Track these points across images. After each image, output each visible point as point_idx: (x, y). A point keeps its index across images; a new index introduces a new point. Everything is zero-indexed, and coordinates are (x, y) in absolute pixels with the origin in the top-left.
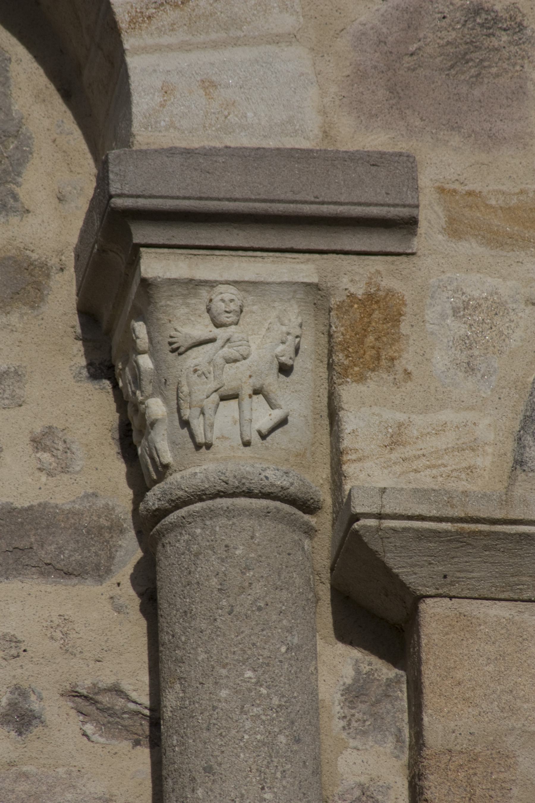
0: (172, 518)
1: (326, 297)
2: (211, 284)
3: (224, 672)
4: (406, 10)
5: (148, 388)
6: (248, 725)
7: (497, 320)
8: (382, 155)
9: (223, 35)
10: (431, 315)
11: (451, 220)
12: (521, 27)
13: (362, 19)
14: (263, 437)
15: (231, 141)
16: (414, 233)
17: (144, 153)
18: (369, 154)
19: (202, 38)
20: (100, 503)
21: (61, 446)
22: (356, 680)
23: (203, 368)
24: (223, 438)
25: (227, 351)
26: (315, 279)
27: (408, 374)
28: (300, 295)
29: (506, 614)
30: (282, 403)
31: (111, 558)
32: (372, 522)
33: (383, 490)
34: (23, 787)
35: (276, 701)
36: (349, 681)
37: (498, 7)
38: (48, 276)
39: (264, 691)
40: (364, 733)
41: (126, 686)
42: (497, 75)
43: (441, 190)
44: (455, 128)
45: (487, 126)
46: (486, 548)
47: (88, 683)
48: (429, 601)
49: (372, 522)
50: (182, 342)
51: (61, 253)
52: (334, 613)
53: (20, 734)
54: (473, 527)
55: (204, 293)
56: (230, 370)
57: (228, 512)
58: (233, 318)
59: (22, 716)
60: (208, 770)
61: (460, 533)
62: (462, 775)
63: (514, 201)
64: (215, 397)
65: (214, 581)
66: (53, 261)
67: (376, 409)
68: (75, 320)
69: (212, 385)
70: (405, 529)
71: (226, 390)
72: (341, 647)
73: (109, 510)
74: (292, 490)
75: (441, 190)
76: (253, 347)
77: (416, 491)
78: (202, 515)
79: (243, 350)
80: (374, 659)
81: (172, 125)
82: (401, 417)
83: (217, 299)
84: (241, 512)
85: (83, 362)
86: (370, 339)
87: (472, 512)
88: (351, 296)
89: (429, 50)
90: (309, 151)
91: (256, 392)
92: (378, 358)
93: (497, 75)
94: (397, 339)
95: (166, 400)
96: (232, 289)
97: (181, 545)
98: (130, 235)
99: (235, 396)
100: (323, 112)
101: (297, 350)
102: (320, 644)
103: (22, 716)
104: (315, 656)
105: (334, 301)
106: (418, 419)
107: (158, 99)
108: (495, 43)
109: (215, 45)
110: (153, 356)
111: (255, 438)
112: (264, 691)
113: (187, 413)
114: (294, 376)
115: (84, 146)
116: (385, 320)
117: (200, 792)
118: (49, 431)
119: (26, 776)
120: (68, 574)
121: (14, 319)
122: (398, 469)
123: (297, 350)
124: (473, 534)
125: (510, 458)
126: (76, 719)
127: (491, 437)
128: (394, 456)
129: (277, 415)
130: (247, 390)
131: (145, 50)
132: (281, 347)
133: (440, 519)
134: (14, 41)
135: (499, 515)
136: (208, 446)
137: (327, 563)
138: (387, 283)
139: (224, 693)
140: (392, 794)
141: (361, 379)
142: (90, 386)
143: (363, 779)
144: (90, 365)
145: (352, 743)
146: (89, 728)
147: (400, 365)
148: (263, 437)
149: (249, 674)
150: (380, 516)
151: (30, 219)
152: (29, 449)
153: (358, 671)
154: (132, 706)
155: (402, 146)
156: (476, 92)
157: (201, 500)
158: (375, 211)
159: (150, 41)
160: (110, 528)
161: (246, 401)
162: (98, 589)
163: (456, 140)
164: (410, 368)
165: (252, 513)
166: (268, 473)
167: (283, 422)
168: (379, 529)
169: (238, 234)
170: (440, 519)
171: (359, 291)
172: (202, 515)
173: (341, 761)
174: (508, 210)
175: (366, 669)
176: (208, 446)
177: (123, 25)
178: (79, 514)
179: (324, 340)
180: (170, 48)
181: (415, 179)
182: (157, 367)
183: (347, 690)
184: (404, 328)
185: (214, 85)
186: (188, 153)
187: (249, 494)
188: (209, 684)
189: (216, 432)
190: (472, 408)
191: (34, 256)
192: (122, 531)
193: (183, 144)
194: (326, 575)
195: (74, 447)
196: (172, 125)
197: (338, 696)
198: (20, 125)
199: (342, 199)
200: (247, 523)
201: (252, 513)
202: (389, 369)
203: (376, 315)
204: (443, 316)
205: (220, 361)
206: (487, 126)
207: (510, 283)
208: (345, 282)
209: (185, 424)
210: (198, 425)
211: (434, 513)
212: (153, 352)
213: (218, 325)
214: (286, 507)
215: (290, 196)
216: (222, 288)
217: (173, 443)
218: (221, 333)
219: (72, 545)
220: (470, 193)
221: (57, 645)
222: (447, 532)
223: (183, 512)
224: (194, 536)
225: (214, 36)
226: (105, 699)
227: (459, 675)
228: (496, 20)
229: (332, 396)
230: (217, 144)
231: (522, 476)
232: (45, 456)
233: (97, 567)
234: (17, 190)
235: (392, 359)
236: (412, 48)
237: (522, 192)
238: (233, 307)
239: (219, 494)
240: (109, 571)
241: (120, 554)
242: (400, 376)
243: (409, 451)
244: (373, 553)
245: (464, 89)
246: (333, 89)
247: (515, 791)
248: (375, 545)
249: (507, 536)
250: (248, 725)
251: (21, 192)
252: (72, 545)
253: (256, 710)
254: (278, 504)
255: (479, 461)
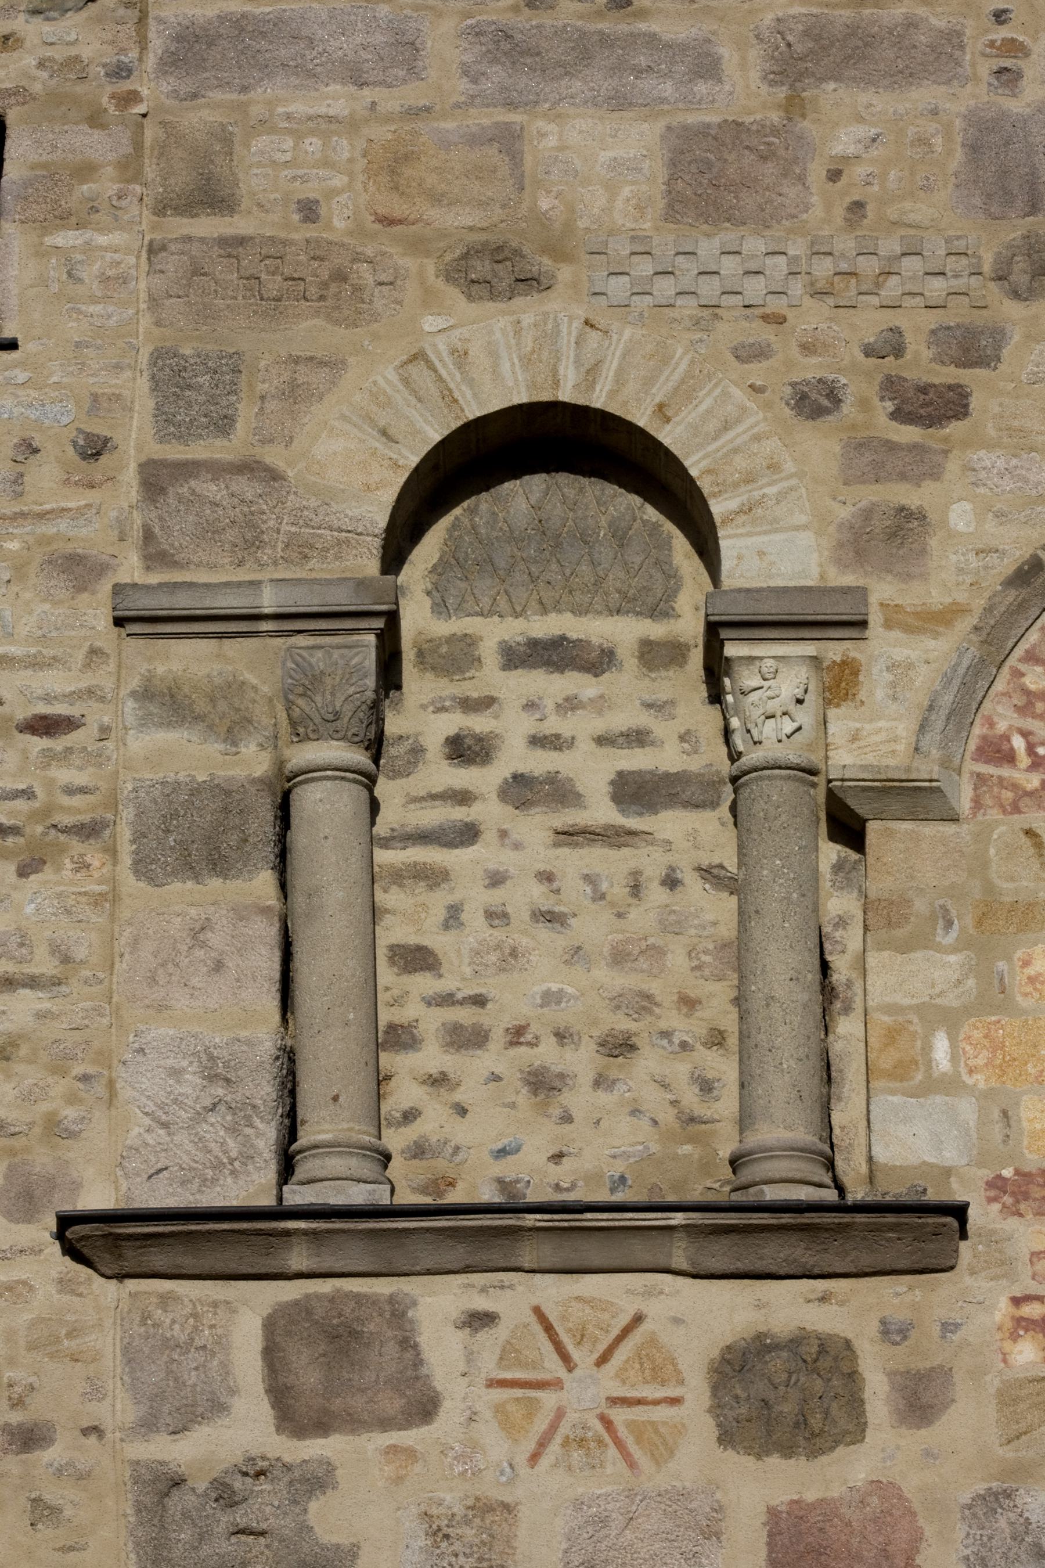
0: (742, 780)
1: (821, 663)
2: (761, 658)
3: (765, 861)
4: (865, 510)
5: (732, 712)
6: (777, 889)
7: (910, 672)
8: (849, 588)
9: (769, 527)
10: (875, 670)
11: (886, 620)
12: (925, 517)
13: (842, 516)
14: (788, 737)
15: (772, 583)
16: (866, 628)
17: (725, 592)
18: (842, 588)
19: (758, 529)
20: (714, 769)
21: (694, 739)
22: (838, 861)
23: (756, 703)
24: (767, 738)
25: (769, 693)
26: (815, 654)
27: (862, 702)
28: (808, 662)
29: (910, 827)
30: (797, 718)
31: (720, 797)
32: (838, 783)
33: (844, 766)
34: (673, 917)
35: (792, 876)
36: (834, 862)
37: (912, 507)
38: (689, 650)
39: (786, 871)
40: (842, 888)
41: (726, 864)
42: (912, 543)
43: (882, 604)
44: (890, 571)
45: (906, 570)
46: (898, 794)
47: (707, 863)
48: (870, 822)
49: (838, 783)
50: (746, 689)
51: (696, 637)
52: (828, 827)
53: (671, 890)
54: (891, 784)
55: (757, 663)
56: (770, 703)
57: (769, 778)
58: (772, 676)
59: (672, 881)
60: (757, 912)
61: (884, 787)
62: (885, 912)
63: (919, 609)
64: (763, 717)
65: (762, 814)
66: (692, 642)
67: (845, 722)
68: (702, 673)
69: (761, 711)
70: (856, 786)
71: (768, 714)
72: (831, 844)
73: (718, 772)
74: (803, 765)
75: (882, 604)
76: (783, 690)
77: (861, 766)
78: (756, 779)
79: (777, 692)
80: (848, 850)
81: (742, 576)
82: (858, 725)
83: (763, 666)
84: (775, 777)
85: (706, 695)
86: (843, 684)
87: (890, 776)
88: (834, 662)
89: (877, 531)
90: (811, 587)
91: (784, 714)
92: (847, 694)
93: (912, 543)
94: (857, 684)
95: (739, 718)
96: (772, 661)
97: (746, 795)
98: (718, 634)
99: (773, 716)
100: (821, 565)
101: (806, 691)
102: (821, 843)
103: (672, 881)
104: (817, 849)
105: (825, 665)
106: (867, 726)
107: (735, 562)
108: (911, 526)
109: (765, 533)
110: (733, 696)
111: (784, 738)
112: (786, 871)
113: (749, 726)
114: (805, 704)
115: (709, 581)
116: (851, 674)
117: (753, 923)
118: (688, 732)
119: (674, 911)
120: (697, 806)
121: (671, 673)
122: (856, 753)
123: (806, 691)
124: (891, 787)
125: (914, 745)
126: (701, 881)
127: (904, 734)
128: (854, 746)
129: (795, 725)
130: (779, 713)
131: (729, 537)
132: (797, 690)
133: (874, 781)
134: (674, 527)
135: (904, 777)
136: (760, 743)
137: (824, 800)
138: (853, 654)
139: (765, 872)
140: (855, 920)
141: (838, 706)
142: (709, 707)
143: (840, 912)
144: (710, 696)
145: (835, 894)
146: (707, 886)
147: (858, 697)
148: (788, 737)
149: (778, 862)
150: (843, 780)
151: (680, 620)
152: (678, 742)
153: (839, 857)
154: (729, 874)
155: (860, 583)
156: (901, 552)
157: (756, 771)
158: (845, 618)
159: (732, 532)
160: (719, 782)
161: (779, 719)
162: (713, 814)
163: (889, 578)
164: (864, 699)
165: (782, 778)
166: (790, 757)
167: (799, 729)
168: (842, 787)
169: (393, 830)
170: (874, 781)
171: (838, 659)
172: (756, 779)
173: (829, 904)
174: (916, 614)
175: (843, 855)
176: (760, 743)
177: (718, 525)
178: (703, 775)
179: (821, 685)
180: (742, 535)
181: (866, 600)
182: (735, 701)
183: (834, 866)
184: (861, 678)
185: (764, 554)
186: (748, 591)
187: (780, 768)
188: (758, 868)
189: (764, 735)
190: (895, 719)
191: (682, 640)
192: (725, 783)
193: (747, 586)
194: (823, 807)
195: (701, 740)
196: (742, 576)
197: (829, 870)
198: (677, 571)
199: (828, 612)
200: (779, 783)
201: (782, 778)
202: (853, 700)
203: (847, 671)
204: (881, 671)
205: (765, 698)
206: (906, 570)
207: (916, 653)
208: (831, 655)
209: (748, 731)
210: (755, 732)
211: (871, 777)
212: (733, 693)
213: (765, 680)
214: (800, 774)
215: (801, 612)
216: (766, 660)
217: (744, 741)
218: (766, 684)
219: (699, 791)
220: (896, 606)
221: (691, 844)
222: (877, 787)
223: (746, 777)
224: (752, 789)
225: (764, 528)
226: (715, 871)
227: (885, 860)
228: (912, 514)
229: (824, 714)
230: (765, 585)
231: (917, 756)
232: (686, 745)
233: (712, 802)
234: (674, 605)
235: (854, 695)
236: (868, 530)
237: (924, 604)
238: (771, 670)
239: (764, 768)
240: (718, 804)
241: (724, 795)
242: (858, 704)
243: (862, 743)
244: (840, 799)
245: (894, 551)
246: (826, 553)
247: (912, 919)
248: (841, 795)
249: (908, 788)
250: (777, 889)
251: (676, 606)
252: (699, 791)
253: (781, 881)
254: (795, 772)
255: (898, 748)
